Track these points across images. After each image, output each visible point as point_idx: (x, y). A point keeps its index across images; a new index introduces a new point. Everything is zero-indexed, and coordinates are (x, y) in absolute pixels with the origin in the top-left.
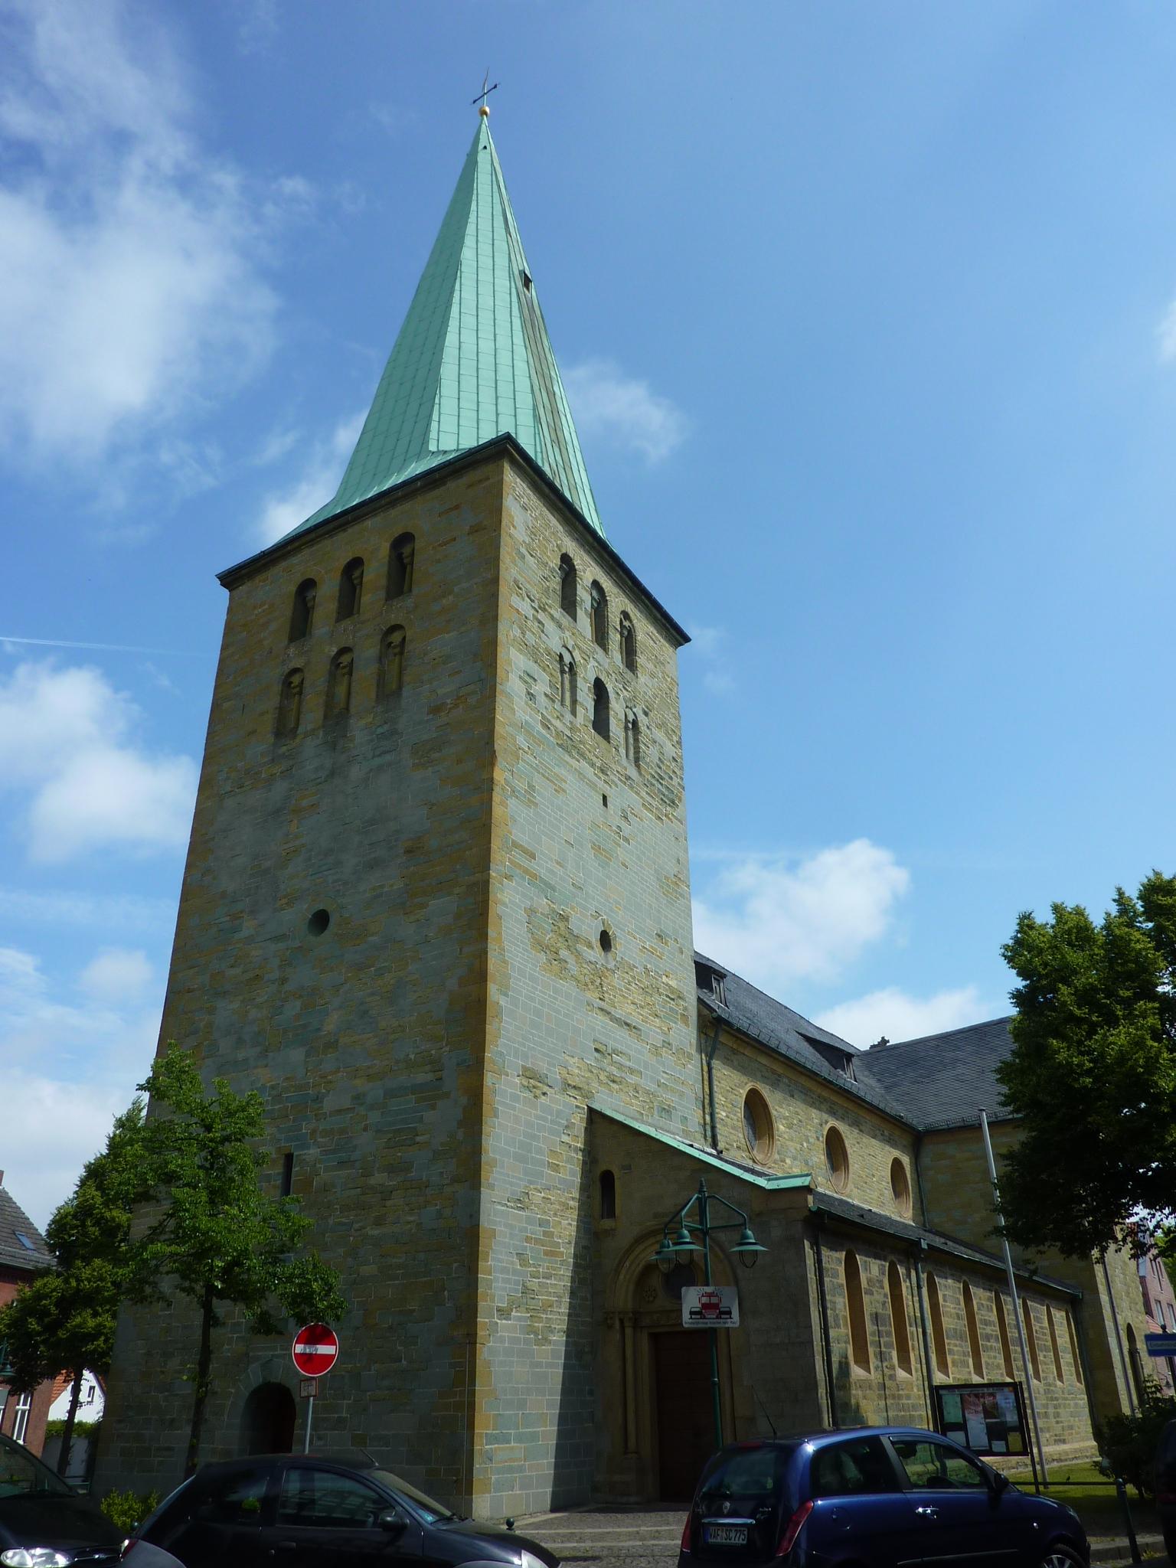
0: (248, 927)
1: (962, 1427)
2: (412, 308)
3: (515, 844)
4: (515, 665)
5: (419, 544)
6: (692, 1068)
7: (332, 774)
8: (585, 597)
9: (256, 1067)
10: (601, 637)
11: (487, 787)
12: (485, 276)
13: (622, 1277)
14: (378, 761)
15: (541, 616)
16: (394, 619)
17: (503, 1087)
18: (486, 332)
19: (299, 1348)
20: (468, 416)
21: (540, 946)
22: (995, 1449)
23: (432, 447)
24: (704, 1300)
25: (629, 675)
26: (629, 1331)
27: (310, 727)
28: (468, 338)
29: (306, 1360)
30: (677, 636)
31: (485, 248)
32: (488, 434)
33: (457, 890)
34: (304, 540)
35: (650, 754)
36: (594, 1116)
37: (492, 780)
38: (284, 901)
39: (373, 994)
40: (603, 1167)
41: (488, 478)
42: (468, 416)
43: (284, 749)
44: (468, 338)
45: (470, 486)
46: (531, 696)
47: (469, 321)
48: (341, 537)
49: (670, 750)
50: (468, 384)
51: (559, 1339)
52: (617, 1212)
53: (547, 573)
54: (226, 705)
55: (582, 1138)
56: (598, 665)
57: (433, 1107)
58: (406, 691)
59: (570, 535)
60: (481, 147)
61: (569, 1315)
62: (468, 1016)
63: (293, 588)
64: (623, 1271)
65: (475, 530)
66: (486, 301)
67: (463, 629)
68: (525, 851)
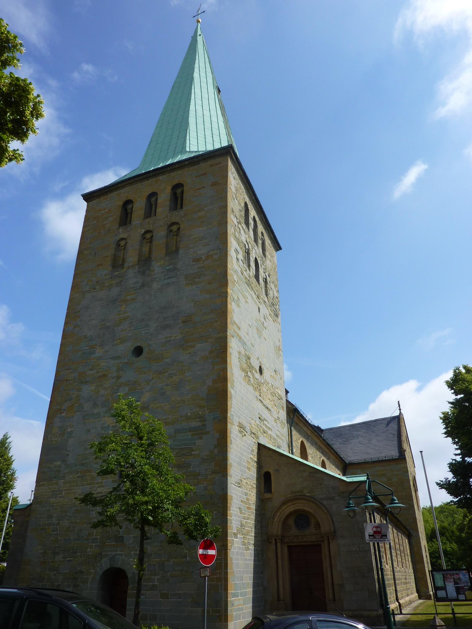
0: (99, 352)
1: (444, 588)
2: (171, 94)
3: (235, 323)
4: (233, 245)
5: (185, 189)
6: (285, 430)
7: (143, 285)
8: (251, 222)
9: (104, 417)
10: (256, 241)
11: (225, 295)
12: (204, 85)
13: (275, 520)
14: (166, 281)
15: (240, 226)
16: (174, 220)
17: (233, 431)
18: (206, 107)
19: (201, 551)
20: (201, 140)
21: (243, 370)
22: (460, 598)
23: (188, 149)
24: (374, 529)
25: (264, 259)
26: (279, 545)
27: (130, 265)
28: (199, 108)
29: (205, 557)
30: (277, 247)
31: (203, 74)
32: (225, 144)
33: (210, 340)
34: (127, 182)
35: (271, 293)
36: (261, 447)
37: (227, 292)
38: (118, 341)
39: (167, 385)
40: (265, 470)
41: (220, 163)
42: (201, 140)
43: (117, 273)
44: (199, 108)
45: (211, 166)
46: (238, 259)
47: (199, 102)
48: (146, 183)
49: (276, 294)
50: (200, 127)
51: (252, 547)
52: (273, 490)
53: (241, 209)
54: (86, 252)
55: (256, 457)
56: (256, 252)
57: (201, 438)
58: (181, 252)
59: (247, 194)
60: (198, 34)
61: (255, 537)
62: (217, 397)
63: (121, 203)
64: (277, 517)
65: (214, 184)
66: (205, 95)
67: (210, 226)
68: (237, 326)
